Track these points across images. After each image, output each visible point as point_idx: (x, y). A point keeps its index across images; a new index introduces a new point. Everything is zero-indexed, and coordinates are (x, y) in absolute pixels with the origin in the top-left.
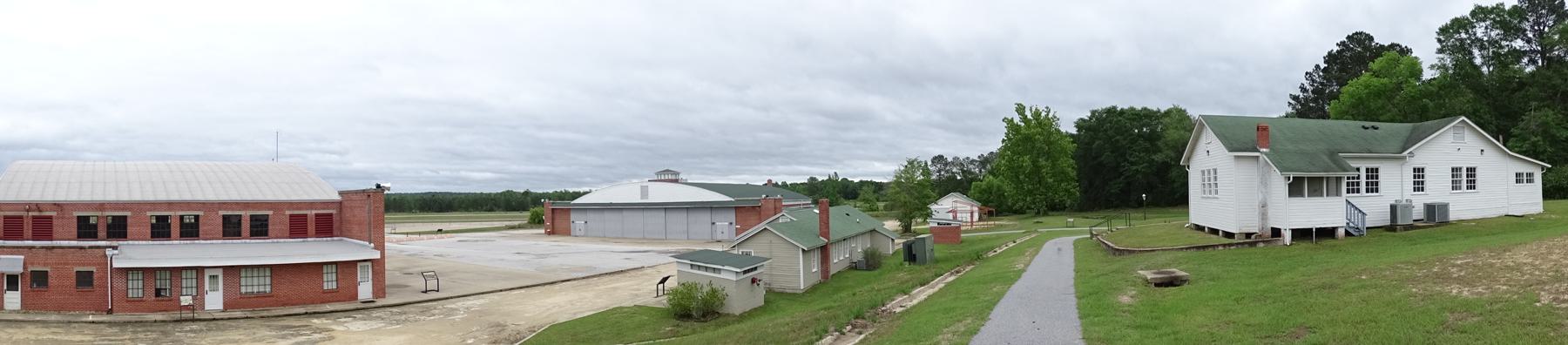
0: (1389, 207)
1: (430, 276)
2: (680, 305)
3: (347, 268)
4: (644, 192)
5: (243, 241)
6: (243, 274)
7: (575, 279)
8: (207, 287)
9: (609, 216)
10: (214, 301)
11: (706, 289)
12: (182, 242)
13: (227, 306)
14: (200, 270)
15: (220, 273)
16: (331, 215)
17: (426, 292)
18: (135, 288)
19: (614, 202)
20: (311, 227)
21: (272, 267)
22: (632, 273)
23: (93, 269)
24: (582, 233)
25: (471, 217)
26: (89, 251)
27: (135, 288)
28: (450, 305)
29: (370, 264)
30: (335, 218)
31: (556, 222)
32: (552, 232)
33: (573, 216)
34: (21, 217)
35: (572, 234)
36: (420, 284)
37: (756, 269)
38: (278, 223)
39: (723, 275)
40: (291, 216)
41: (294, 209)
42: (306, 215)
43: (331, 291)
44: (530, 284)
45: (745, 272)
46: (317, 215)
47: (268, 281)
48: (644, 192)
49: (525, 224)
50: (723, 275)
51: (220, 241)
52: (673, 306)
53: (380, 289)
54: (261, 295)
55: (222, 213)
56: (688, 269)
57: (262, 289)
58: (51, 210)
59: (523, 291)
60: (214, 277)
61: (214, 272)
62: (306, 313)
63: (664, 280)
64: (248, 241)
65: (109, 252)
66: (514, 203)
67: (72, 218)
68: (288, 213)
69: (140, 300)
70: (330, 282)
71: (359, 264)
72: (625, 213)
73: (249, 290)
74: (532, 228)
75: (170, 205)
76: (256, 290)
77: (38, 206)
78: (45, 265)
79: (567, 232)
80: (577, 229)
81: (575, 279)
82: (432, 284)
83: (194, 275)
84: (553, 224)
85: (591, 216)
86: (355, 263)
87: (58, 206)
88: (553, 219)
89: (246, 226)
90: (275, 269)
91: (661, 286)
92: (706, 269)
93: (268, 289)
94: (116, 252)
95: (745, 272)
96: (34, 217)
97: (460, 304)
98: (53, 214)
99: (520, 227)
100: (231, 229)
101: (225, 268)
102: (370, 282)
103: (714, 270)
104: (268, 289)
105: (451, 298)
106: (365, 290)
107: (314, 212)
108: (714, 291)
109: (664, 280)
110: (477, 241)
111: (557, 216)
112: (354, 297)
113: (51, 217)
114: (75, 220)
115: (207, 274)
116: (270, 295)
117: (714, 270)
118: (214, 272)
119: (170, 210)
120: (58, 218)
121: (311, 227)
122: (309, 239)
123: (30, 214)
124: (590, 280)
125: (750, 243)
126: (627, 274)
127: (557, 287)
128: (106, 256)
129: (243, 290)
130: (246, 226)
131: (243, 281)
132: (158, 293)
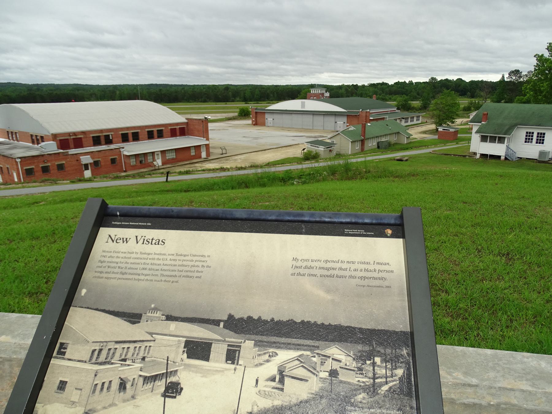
0: (212, 356)
1: (223, 149)
2: (306, 157)
3: (198, 148)
4: (303, 105)
5: (155, 140)
6: (167, 153)
7: (272, 149)
8: (156, 158)
9: (285, 117)
10: (159, 162)
11: (314, 152)
12: (134, 143)
13: (163, 164)
14: (153, 153)
15: (160, 153)
16: (184, 127)
17: (222, 154)
18: (133, 162)
19: (287, 109)
20: (178, 133)
21: (175, 149)
22: (294, 146)
23: (117, 157)
24: (271, 125)
25: (200, 108)
26: (114, 150)
27: (133, 162)
28: (236, 157)
29: (205, 146)
30: (186, 129)
31: (258, 119)
32: (256, 124)
33: (267, 116)
34: (67, 139)
35: (266, 125)
36: (220, 151)
37: (331, 147)
38: (166, 131)
39: (320, 149)
40: (171, 129)
41: (172, 126)
42: (176, 128)
43: (193, 156)
44: (257, 150)
45: (327, 148)
46: (179, 128)
47: (174, 154)
48: (303, 105)
49: (236, 116)
50: (320, 149)
51: (147, 141)
52: (304, 157)
53: (208, 154)
54: (173, 159)
55: (147, 130)
56: (310, 146)
57: (173, 157)
58: (81, 135)
59: (255, 153)
60: (158, 154)
61: (157, 153)
62: (190, 163)
63: (304, 149)
64: (157, 140)
65: (122, 150)
66: (220, 97)
67: (90, 137)
68: (170, 128)
69: (135, 166)
70: (193, 153)
71: (201, 146)
72: (293, 115)
73: (169, 158)
74: (241, 119)
75: (128, 128)
76: (171, 157)
77: (75, 134)
78: (99, 158)
79: (263, 124)
80: (269, 123)
81: (272, 149)
82: (224, 151)
83: (151, 155)
84: (256, 120)
85: (276, 117)
86: (200, 146)
87: (83, 133)
88: (256, 117)
89: (155, 134)
90: (176, 150)
91: (303, 151)
92: (315, 146)
93: (175, 157)
94: (124, 149)
95: (327, 148)
96: (73, 139)
97: (239, 157)
98: (82, 136)
99: (234, 119)
100: (150, 136)
101: (161, 151)
102: (205, 152)
103: (317, 147)
104: (175, 157)
105: (231, 156)
106: (204, 155)
107: (178, 127)
108: (317, 153)
109: (304, 149)
110: (219, 130)
111: (259, 116)
112: (200, 157)
113: (81, 138)
114: (91, 138)
115: (156, 153)
116: (176, 159)
117: (317, 147)
118: (157, 153)
119: (128, 130)
120: (84, 138)
121: (178, 133)
122: (178, 137)
123: (72, 137)
124: (278, 149)
125: (334, 138)
126: (293, 147)
127: (267, 151)
128: (120, 151)
129: (167, 158)
130: (155, 134)
131: (167, 155)
132: (141, 162)
